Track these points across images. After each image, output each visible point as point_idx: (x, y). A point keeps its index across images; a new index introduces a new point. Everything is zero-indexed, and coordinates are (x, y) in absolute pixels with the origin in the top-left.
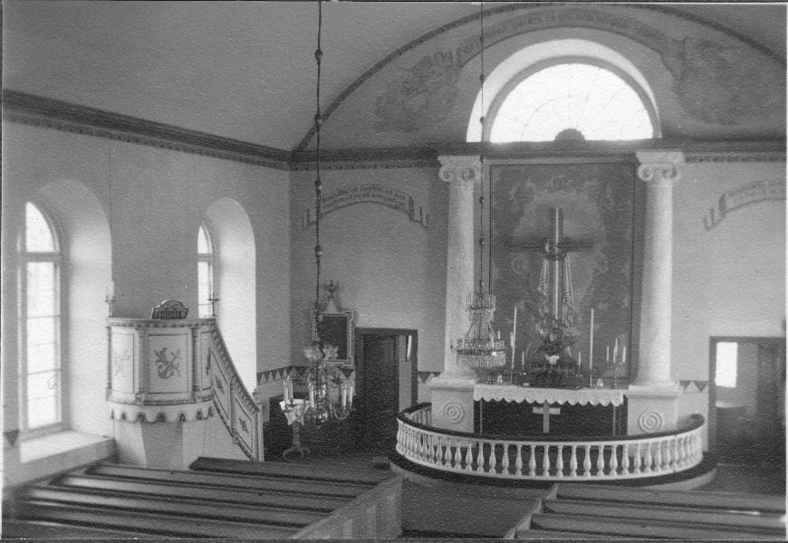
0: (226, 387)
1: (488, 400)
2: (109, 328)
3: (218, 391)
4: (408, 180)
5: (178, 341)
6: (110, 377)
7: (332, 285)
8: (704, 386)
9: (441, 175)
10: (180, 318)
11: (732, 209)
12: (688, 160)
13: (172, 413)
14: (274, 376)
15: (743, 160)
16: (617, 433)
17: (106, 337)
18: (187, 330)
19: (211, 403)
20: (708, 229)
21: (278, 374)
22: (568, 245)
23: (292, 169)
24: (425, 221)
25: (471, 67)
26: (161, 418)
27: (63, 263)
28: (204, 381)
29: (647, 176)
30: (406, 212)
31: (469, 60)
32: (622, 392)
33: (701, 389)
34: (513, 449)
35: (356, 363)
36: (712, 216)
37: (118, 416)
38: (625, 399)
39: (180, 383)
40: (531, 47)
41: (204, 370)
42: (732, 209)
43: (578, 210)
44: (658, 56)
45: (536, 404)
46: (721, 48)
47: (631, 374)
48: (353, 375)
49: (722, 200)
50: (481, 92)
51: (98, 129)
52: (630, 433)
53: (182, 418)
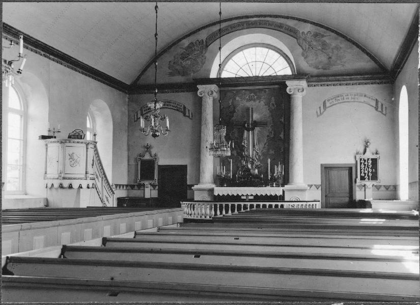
0: (100, 179)
1: (221, 195)
2: (47, 145)
3: (96, 179)
4: (184, 99)
5: (79, 149)
6: (46, 169)
7: (148, 146)
8: (319, 187)
9: (198, 94)
10: (81, 138)
11: (329, 107)
12: (309, 86)
13: (76, 185)
14: (120, 188)
15: (340, 85)
16: (280, 199)
17: (45, 150)
18: (84, 145)
19: (93, 181)
20: (318, 116)
21: (121, 187)
22: (256, 124)
23: (129, 94)
24: (191, 116)
25: (214, 46)
26: (70, 187)
27: (25, 116)
28: (90, 170)
29: (290, 92)
30: (182, 112)
31: (212, 43)
32: (281, 189)
33: (317, 188)
34: (221, 206)
35: (158, 183)
36: (320, 110)
37: (49, 186)
38: (284, 192)
39: (79, 170)
40: (238, 54)
41: (91, 165)
42: (329, 107)
43: (259, 110)
44: (295, 40)
45: (243, 195)
46: (323, 36)
47: (286, 180)
48: (157, 187)
49: (324, 103)
50: (219, 54)
51: (44, 53)
52: (286, 200)
53: (80, 187)
